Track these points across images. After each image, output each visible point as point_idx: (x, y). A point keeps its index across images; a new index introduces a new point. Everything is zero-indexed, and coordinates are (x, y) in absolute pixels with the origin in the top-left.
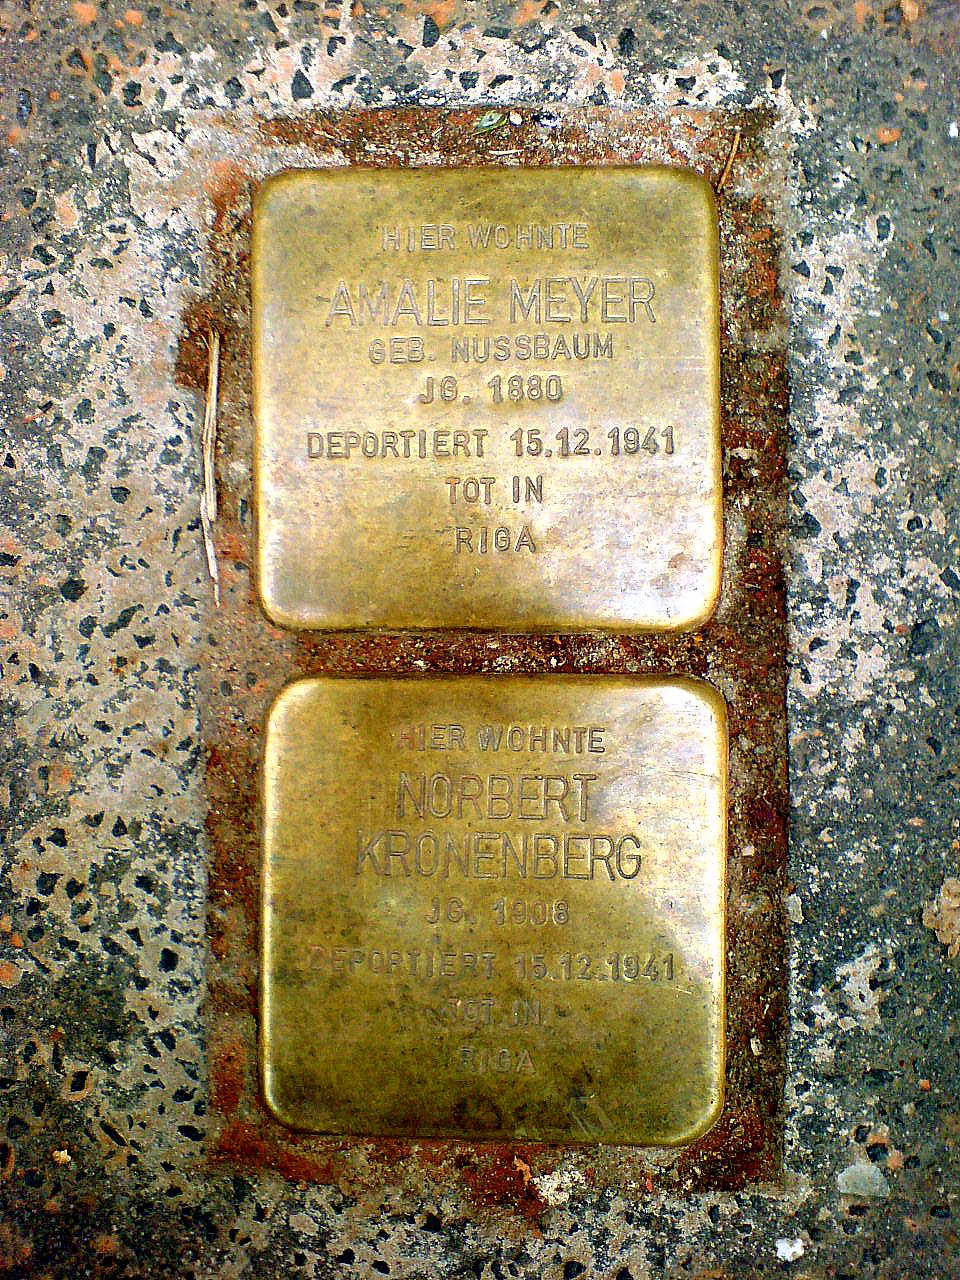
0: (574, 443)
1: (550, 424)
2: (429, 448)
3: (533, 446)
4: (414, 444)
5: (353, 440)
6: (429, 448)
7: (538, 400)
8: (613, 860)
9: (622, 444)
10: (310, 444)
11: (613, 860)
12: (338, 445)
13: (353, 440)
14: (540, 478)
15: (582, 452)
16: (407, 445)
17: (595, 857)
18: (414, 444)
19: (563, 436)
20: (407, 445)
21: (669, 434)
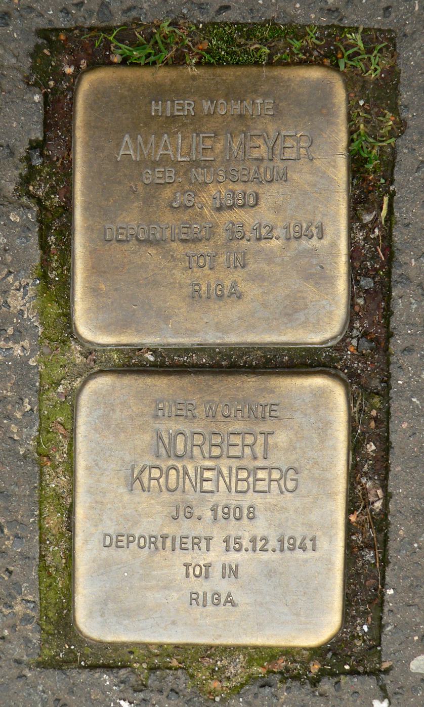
0: (260, 544)
1: (246, 531)
2: (178, 546)
3: (237, 546)
4: (169, 543)
5: (131, 539)
6: (178, 546)
7: (220, 297)
8: (282, 482)
9: (286, 545)
10: (104, 539)
11: (282, 482)
12: (49, 446)
13: (131, 539)
14: (237, 566)
15: (263, 550)
16: (164, 543)
17: (151, 479)
18: (169, 543)
19: (253, 540)
20: (164, 543)
21: (313, 540)
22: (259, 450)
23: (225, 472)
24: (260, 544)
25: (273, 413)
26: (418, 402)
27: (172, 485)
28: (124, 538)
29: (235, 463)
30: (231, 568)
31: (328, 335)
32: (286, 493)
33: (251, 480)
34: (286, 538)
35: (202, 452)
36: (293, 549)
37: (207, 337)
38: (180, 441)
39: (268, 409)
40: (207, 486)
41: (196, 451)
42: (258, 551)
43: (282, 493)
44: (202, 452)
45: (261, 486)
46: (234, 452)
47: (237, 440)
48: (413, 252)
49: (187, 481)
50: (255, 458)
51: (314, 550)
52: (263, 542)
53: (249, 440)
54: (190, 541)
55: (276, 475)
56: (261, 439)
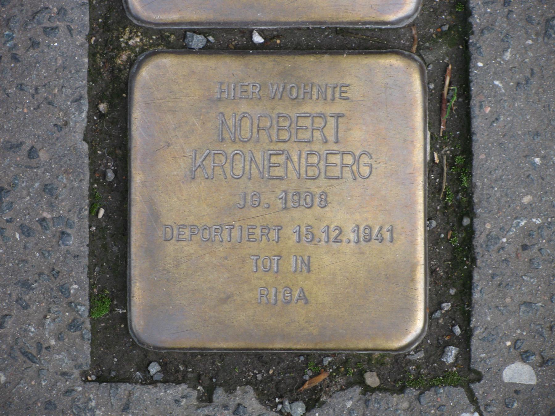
22: (330, 134)
23: (295, 157)
24: (334, 234)
25: (343, 95)
26: (500, 85)
27: (239, 172)
28: (187, 231)
29: (306, 148)
30: (303, 261)
31: (400, 14)
32: (359, 179)
33: (322, 165)
34: (362, 228)
35: (270, 136)
36: (369, 240)
37: (479, 120)
38: (246, 124)
39: (338, 90)
40: (278, 172)
41: (264, 135)
42: (331, 243)
43: (355, 179)
44: (270, 136)
45: (336, 172)
46: (307, 135)
47: (308, 122)
48: (518, 192)
49: (254, 166)
50: (326, 142)
51: (391, 242)
52: (337, 232)
53: (319, 122)
54: (258, 231)
55: (349, 160)
56: (332, 122)
